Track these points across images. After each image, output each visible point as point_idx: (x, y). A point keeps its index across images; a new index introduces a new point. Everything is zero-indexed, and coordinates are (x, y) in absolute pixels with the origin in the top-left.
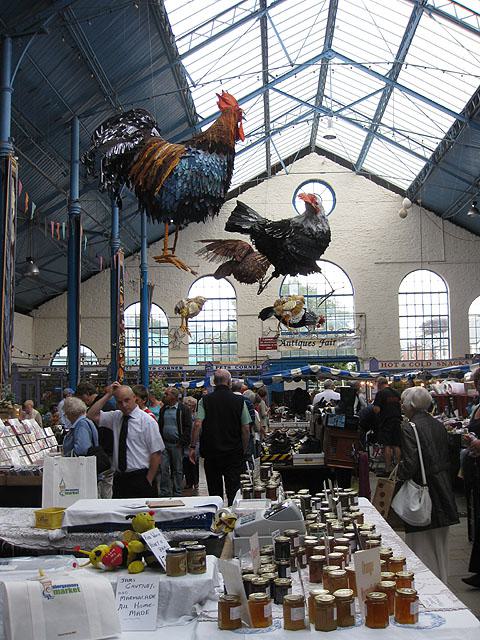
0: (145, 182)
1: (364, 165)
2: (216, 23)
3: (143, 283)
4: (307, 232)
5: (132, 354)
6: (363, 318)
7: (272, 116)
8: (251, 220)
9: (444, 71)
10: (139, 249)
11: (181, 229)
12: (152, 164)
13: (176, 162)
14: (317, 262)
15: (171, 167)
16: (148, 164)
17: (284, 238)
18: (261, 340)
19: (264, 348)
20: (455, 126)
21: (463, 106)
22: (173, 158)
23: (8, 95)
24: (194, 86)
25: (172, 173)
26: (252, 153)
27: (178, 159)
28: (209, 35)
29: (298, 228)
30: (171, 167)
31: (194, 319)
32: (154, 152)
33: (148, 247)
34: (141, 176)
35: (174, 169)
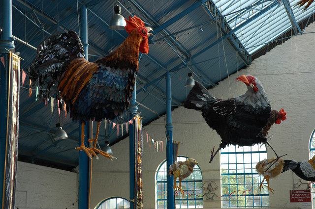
0: (68, 93)
1: (250, 53)
3: (169, 141)
8: (203, 99)
10: (164, 113)
12: (73, 80)
15: (85, 82)
16: (70, 80)
17: (227, 115)
18: (292, 193)
19: (296, 201)
22: (88, 74)
23: (28, 44)
25: (85, 86)
29: (241, 106)
30: (85, 82)
31: (185, 179)
32: (75, 70)
33: (173, 109)
34: (66, 89)
35: (88, 83)
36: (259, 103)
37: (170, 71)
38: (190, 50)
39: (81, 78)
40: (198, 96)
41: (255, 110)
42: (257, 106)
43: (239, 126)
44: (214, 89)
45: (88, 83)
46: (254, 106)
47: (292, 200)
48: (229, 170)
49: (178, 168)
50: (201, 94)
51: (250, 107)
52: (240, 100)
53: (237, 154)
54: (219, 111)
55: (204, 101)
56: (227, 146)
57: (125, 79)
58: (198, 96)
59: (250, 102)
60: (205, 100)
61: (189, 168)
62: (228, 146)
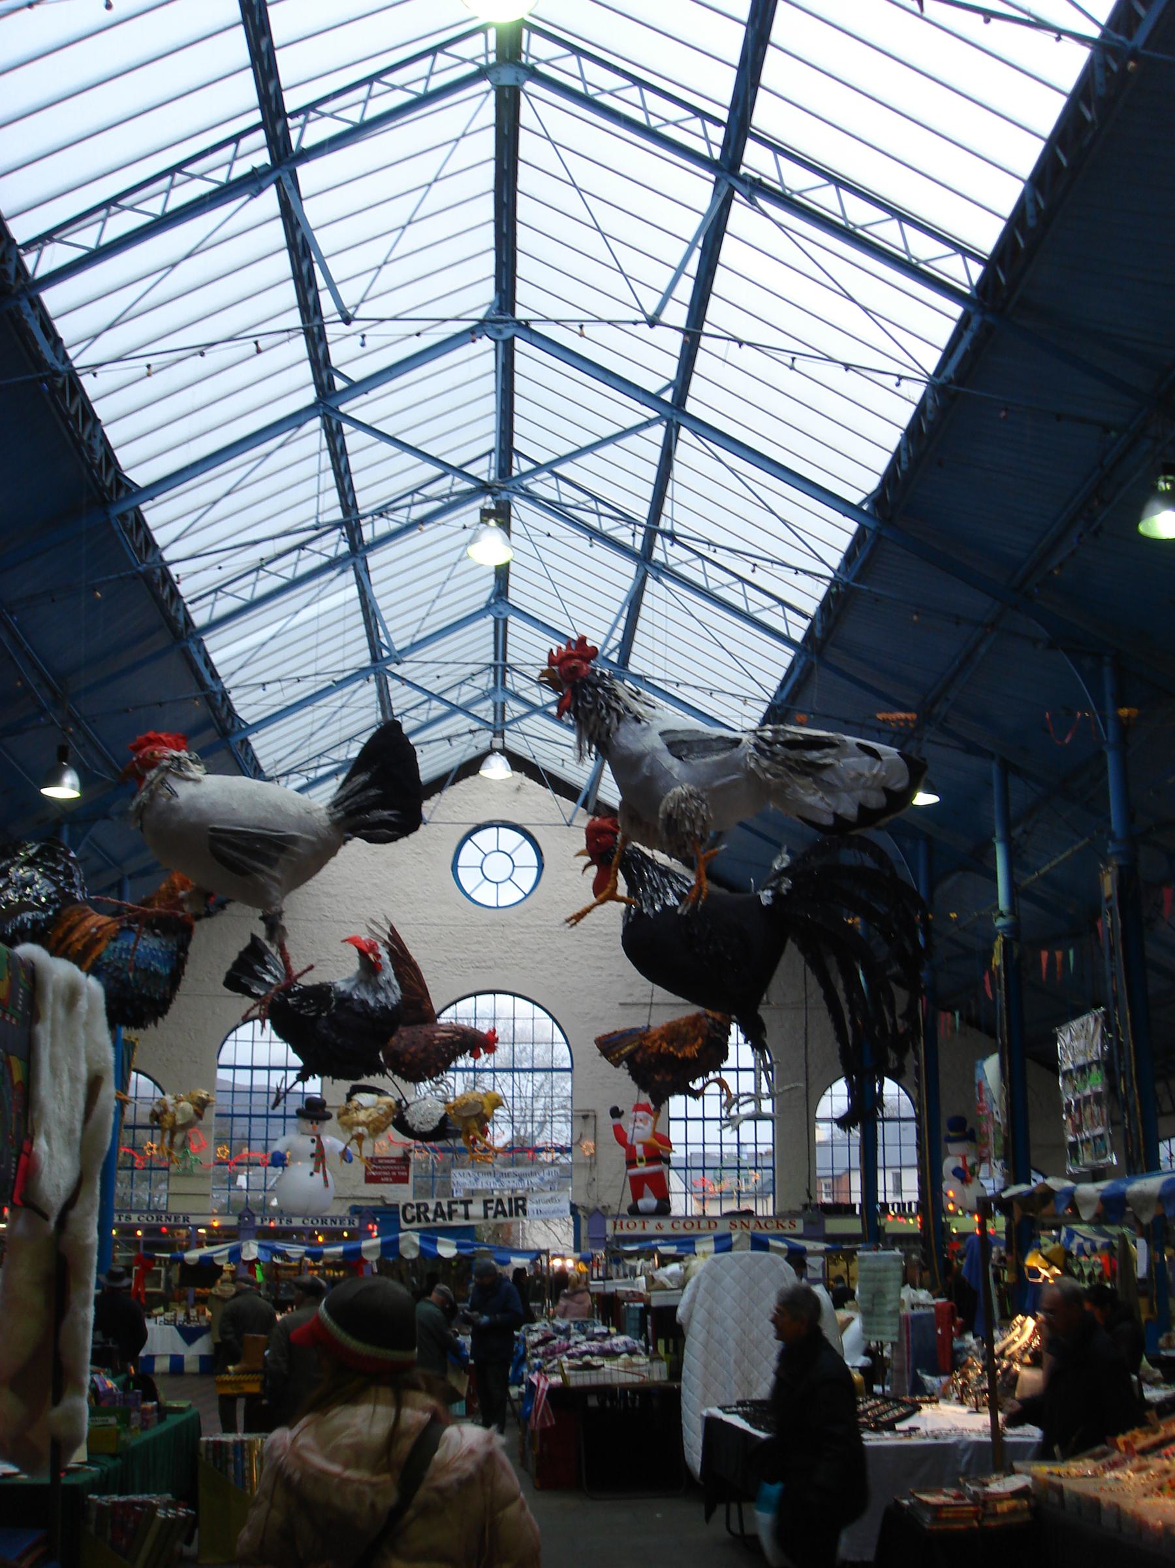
2: (442, 60)
4: (358, 1008)
5: (671, 1341)
6: (591, 1121)
7: (521, 459)
8: (268, 978)
9: (847, 367)
11: (209, 914)
13: (100, 948)
14: (440, 1021)
17: (318, 1017)
20: (858, 539)
21: (872, 483)
22: (99, 940)
24: (347, 320)
26: (429, 621)
27: (105, 942)
28: (419, 88)
29: (345, 999)
32: (71, 929)
36: (381, 996)
37: (130, 877)
38: (539, 1043)
39: (85, 946)
40: (257, 967)
41: (373, 1010)
42: (378, 1001)
43: (339, 1041)
44: (215, 919)
45: (99, 958)
46: (372, 1003)
47: (370, 1179)
48: (704, 1144)
49: (171, 1109)
50: (264, 964)
51: (364, 1003)
52: (342, 986)
53: (255, 1072)
54: (300, 1007)
55: (270, 984)
56: (311, 1078)
57: (172, 953)
58: (257, 967)
59: (361, 994)
60: (272, 981)
61: (195, 1111)
62: (156, 1024)
